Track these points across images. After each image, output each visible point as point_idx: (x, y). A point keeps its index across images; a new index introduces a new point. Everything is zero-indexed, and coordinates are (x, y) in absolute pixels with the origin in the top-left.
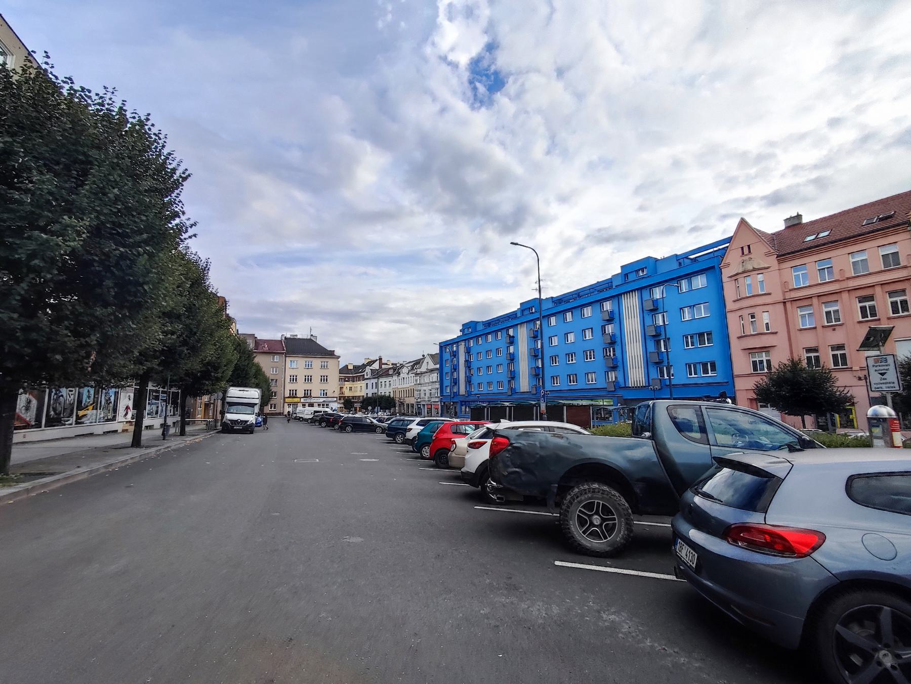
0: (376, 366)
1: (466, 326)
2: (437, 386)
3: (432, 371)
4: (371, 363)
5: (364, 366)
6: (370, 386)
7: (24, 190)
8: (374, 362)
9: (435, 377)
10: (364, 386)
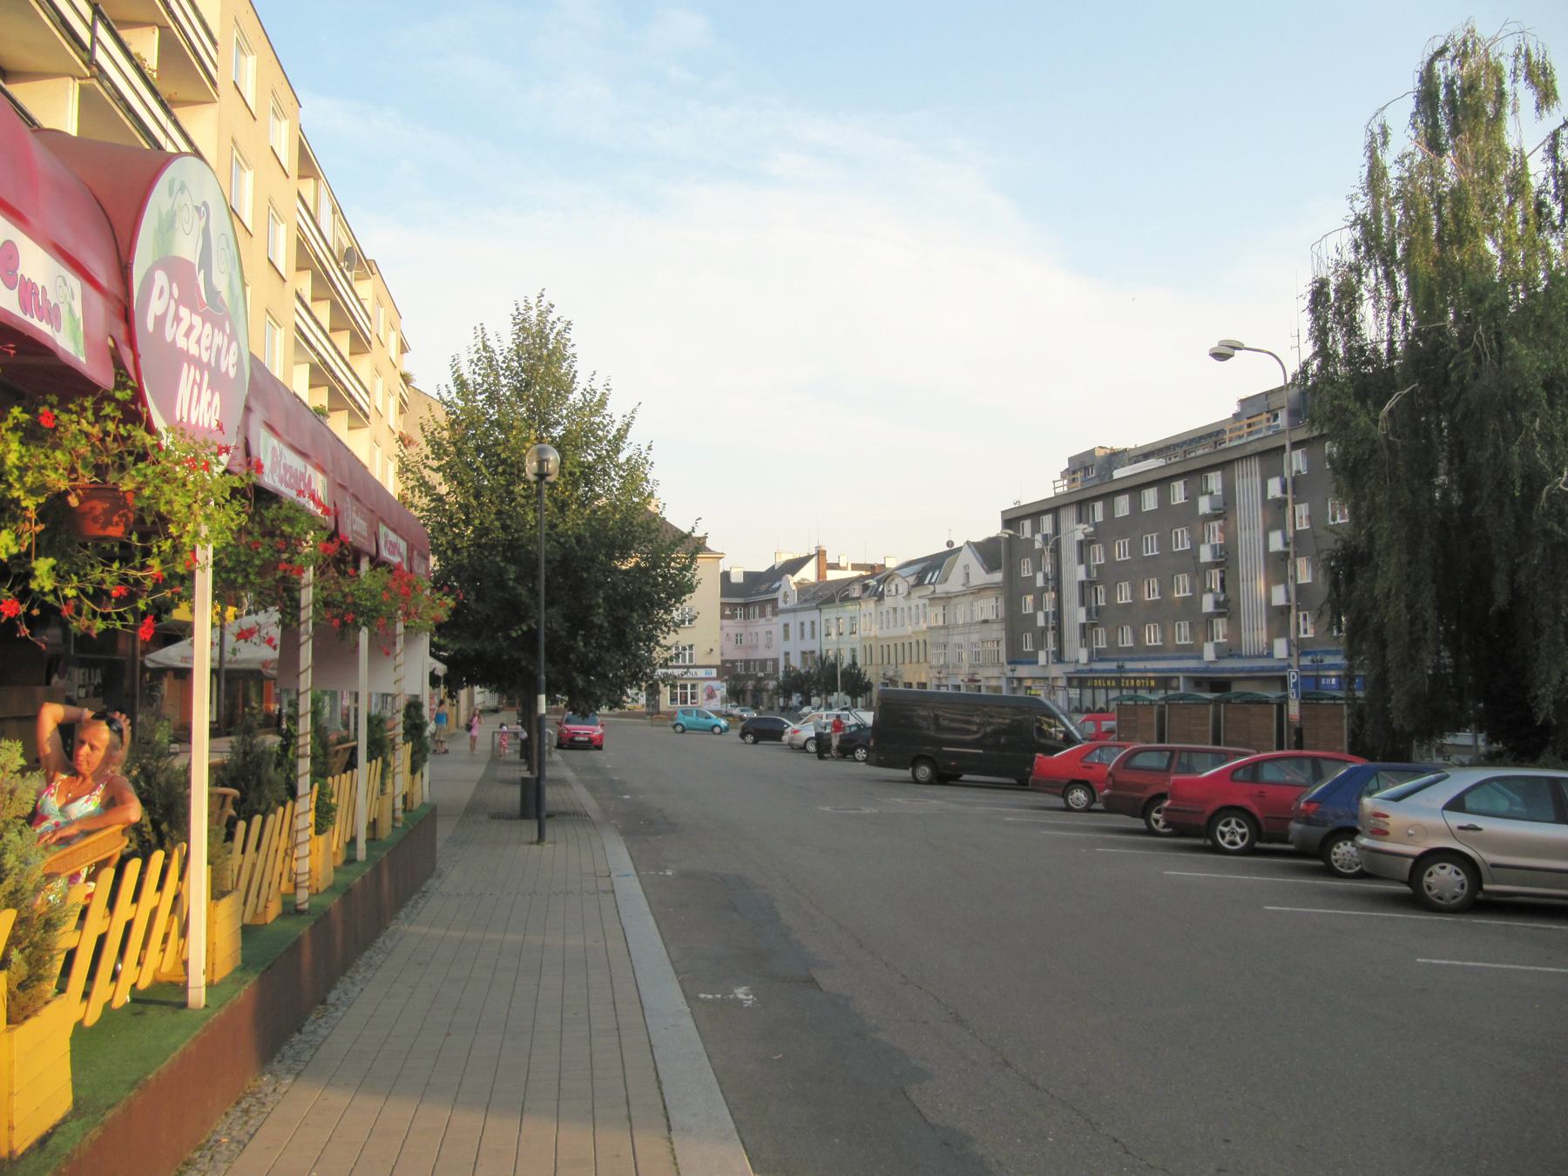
0: (808, 573)
1: (1081, 465)
2: (997, 631)
3: (980, 590)
4: (795, 565)
5: (777, 573)
6: (794, 631)
7: (1455, 118)
8: (808, 558)
9: (988, 607)
10: (778, 631)
